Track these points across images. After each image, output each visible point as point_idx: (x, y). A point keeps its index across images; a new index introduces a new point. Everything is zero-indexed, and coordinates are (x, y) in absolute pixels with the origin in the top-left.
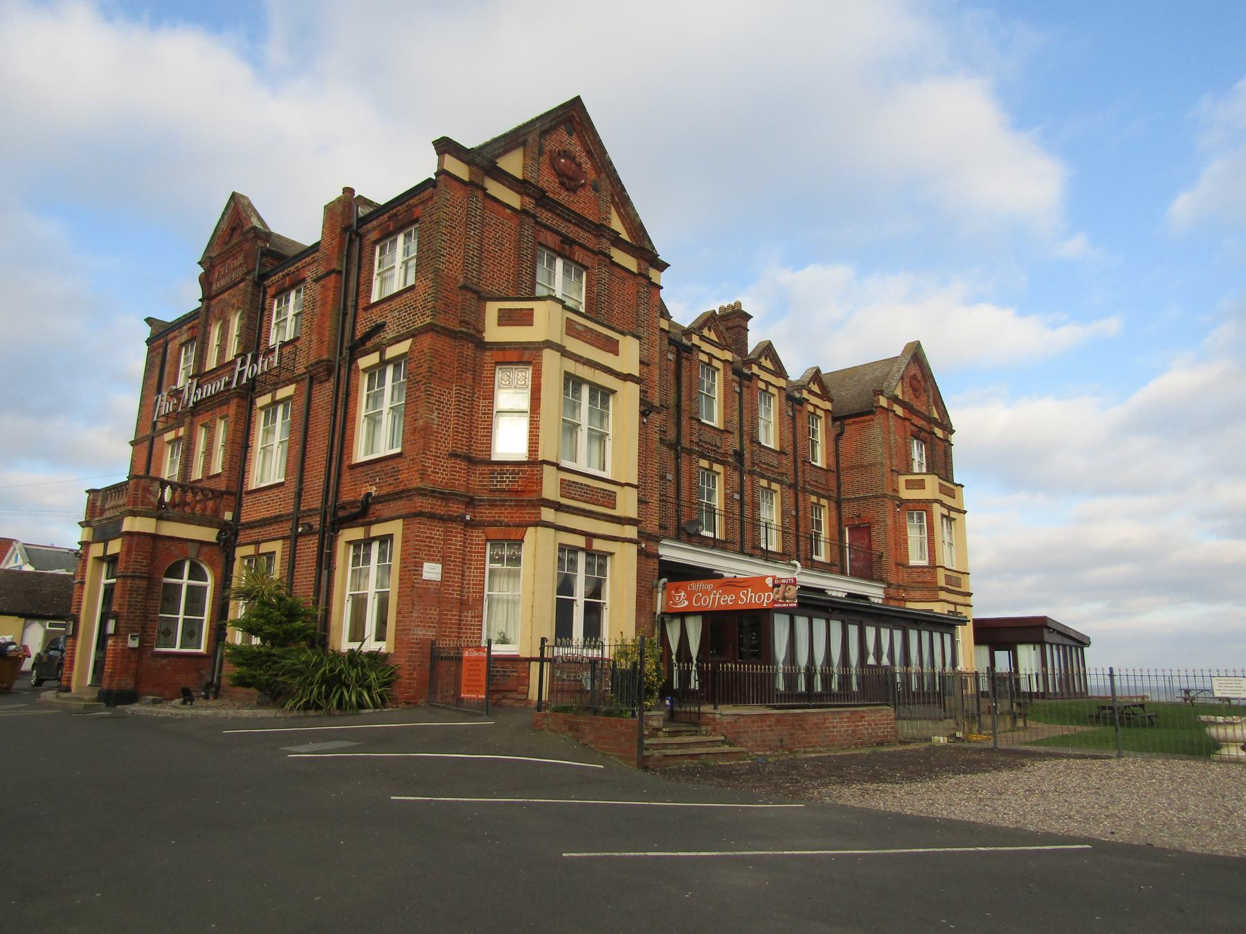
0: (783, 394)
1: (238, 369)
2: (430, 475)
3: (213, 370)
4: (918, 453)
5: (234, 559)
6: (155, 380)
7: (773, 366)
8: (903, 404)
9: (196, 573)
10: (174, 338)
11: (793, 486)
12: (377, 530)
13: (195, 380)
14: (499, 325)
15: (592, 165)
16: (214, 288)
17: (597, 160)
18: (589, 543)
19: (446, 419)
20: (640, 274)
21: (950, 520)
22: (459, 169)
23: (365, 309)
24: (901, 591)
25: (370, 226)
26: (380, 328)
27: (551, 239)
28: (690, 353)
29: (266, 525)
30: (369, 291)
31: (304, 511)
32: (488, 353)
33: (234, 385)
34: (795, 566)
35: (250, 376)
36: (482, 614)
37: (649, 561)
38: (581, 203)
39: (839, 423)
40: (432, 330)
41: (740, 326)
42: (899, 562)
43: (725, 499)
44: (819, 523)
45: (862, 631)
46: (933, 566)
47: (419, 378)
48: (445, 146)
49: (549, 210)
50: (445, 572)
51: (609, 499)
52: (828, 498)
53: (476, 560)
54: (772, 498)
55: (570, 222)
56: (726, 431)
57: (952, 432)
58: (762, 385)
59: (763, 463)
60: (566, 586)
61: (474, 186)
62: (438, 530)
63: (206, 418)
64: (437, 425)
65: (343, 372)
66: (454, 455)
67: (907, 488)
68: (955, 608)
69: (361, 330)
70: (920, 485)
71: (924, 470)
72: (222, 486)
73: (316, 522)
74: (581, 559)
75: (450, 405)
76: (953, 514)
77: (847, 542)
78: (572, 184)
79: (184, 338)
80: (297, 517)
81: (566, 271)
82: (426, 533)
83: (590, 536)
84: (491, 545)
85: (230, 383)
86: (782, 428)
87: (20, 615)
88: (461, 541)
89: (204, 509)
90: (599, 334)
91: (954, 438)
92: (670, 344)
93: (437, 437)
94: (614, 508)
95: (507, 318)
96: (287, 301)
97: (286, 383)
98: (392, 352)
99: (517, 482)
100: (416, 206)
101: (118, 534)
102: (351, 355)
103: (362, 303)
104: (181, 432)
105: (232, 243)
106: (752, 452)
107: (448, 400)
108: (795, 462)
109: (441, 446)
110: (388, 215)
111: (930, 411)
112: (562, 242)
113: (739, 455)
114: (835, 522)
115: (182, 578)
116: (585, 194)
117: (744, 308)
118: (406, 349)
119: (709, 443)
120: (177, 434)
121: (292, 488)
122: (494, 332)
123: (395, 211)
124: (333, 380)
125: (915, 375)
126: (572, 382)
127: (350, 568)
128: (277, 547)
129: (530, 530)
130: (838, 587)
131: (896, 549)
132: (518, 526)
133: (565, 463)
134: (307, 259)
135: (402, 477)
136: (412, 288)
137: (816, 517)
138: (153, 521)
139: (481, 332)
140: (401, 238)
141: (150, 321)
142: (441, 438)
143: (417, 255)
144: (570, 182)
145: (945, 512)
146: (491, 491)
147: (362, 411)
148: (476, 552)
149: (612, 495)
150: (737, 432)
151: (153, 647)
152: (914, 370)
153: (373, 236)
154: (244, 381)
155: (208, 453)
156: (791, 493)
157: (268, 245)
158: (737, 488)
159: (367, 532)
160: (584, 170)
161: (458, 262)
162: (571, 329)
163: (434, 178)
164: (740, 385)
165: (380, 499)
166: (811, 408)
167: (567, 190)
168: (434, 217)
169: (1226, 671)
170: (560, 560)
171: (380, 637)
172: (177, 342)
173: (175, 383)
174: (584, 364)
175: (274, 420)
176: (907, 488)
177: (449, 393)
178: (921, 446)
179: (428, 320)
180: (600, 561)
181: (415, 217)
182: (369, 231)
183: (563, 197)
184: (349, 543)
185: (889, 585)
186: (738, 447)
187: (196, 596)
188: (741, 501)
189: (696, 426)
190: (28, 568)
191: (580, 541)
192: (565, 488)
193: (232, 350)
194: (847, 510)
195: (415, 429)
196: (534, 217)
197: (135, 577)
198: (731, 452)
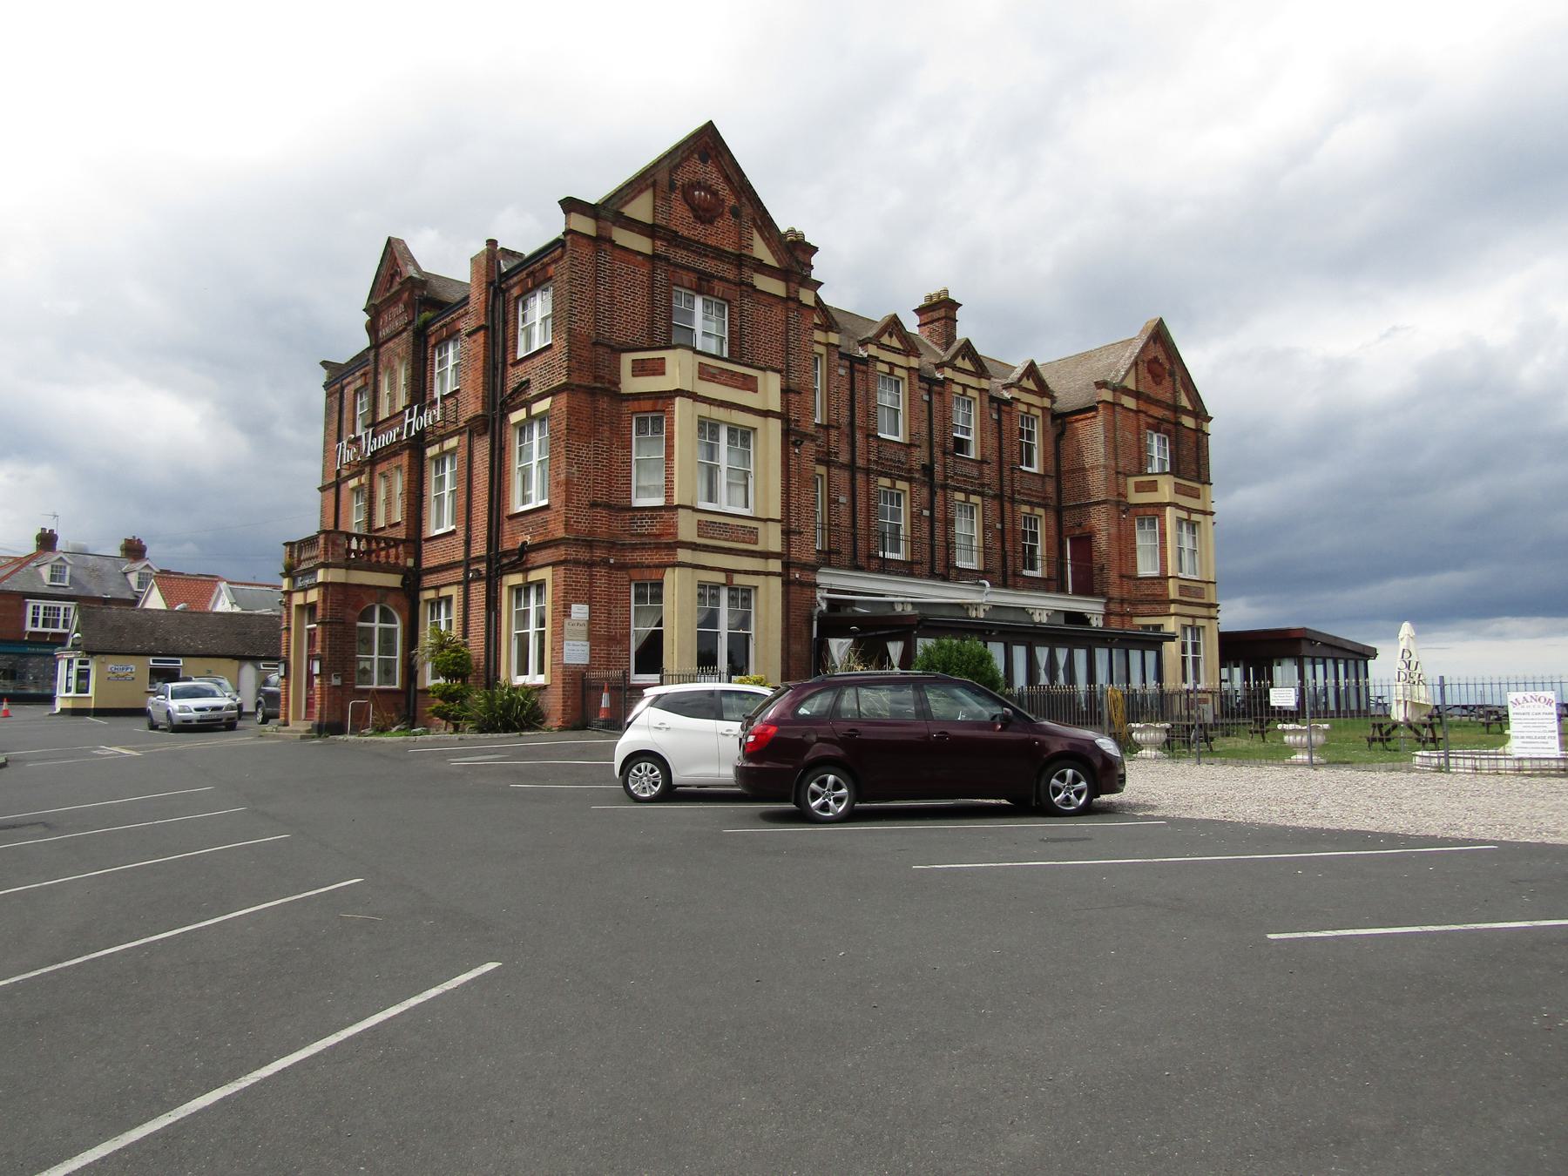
0: (986, 399)
1: (407, 421)
2: (573, 525)
3: (388, 419)
4: (1158, 450)
5: (419, 603)
6: (335, 426)
7: (973, 365)
8: (1136, 395)
9: (386, 617)
10: (349, 383)
11: (1000, 497)
12: (534, 576)
13: (371, 430)
14: (633, 376)
15: (731, 190)
17: (736, 184)
19: (585, 472)
20: (788, 298)
21: (1193, 526)
22: (586, 225)
23: (513, 365)
24: (1125, 606)
25: (512, 282)
26: (526, 384)
27: (687, 278)
28: (867, 365)
29: (443, 570)
30: (515, 346)
31: (473, 558)
32: (625, 404)
33: (405, 437)
34: (984, 585)
35: (418, 429)
36: (630, 648)
37: (805, 589)
38: (721, 235)
39: (1059, 421)
40: (567, 389)
42: (1124, 572)
43: (912, 517)
44: (1034, 536)
45: (1031, 654)
48: (570, 205)
49: (684, 249)
51: (753, 535)
53: (621, 600)
54: (972, 513)
55: (707, 256)
56: (910, 446)
59: (960, 475)
60: (711, 619)
61: (601, 241)
62: (584, 575)
64: (578, 478)
66: (594, 505)
67: (1137, 491)
68: (1194, 622)
69: (511, 385)
72: (401, 533)
73: (483, 567)
74: (724, 595)
75: (590, 458)
76: (1195, 517)
77: (1069, 557)
78: (708, 215)
79: (359, 383)
80: (467, 562)
81: (706, 305)
82: (572, 578)
83: (729, 572)
84: (636, 585)
85: (401, 434)
86: (984, 435)
87: (234, 657)
88: (605, 583)
89: (388, 556)
90: (734, 373)
91: (1211, 428)
92: (841, 358)
93: (577, 489)
94: (756, 543)
95: (641, 369)
96: (447, 351)
97: (451, 435)
98: (538, 408)
99: (656, 526)
100: (549, 264)
103: (510, 361)
104: (364, 479)
105: (393, 290)
107: (587, 454)
109: (583, 497)
110: (525, 272)
112: (699, 279)
113: (928, 470)
114: (1053, 533)
115: (373, 622)
116: (724, 223)
118: (547, 407)
119: (891, 460)
120: (360, 480)
121: (461, 534)
122: (632, 384)
123: (531, 268)
124: (489, 433)
125: (1156, 358)
126: (708, 428)
128: (454, 591)
129: (669, 570)
131: (1120, 560)
132: (658, 566)
134: (460, 311)
136: (549, 347)
137: (1031, 527)
138: (343, 571)
140: (539, 295)
141: (325, 364)
142: (582, 489)
143: (552, 314)
144: (705, 215)
145: (1184, 515)
146: (632, 535)
148: (621, 592)
149: (754, 532)
150: (925, 446)
151: (354, 684)
152: (1157, 352)
153: (515, 292)
154: (413, 433)
155: (389, 502)
157: (425, 293)
160: (722, 197)
161: (590, 319)
162: (705, 373)
163: (562, 237)
164: (930, 393)
166: (1023, 408)
167: (703, 223)
169: (1388, 680)
170: (700, 595)
171: (541, 671)
172: (352, 387)
173: (354, 432)
174: (719, 406)
175: (444, 471)
176: (1137, 491)
177: (588, 447)
178: (1164, 439)
179: (564, 380)
180: (744, 594)
181: (549, 275)
182: (512, 287)
183: (698, 232)
185: (1110, 600)
186: (927, 462)
187: (388, 636)
188: (932, 518)
189: (874, 444)
190: (237, 609)
191: (720, 578)
192: (702, 529)
193: (402, 401)
195: (558, 483)
196: (667, 259)
197: (333, 622)
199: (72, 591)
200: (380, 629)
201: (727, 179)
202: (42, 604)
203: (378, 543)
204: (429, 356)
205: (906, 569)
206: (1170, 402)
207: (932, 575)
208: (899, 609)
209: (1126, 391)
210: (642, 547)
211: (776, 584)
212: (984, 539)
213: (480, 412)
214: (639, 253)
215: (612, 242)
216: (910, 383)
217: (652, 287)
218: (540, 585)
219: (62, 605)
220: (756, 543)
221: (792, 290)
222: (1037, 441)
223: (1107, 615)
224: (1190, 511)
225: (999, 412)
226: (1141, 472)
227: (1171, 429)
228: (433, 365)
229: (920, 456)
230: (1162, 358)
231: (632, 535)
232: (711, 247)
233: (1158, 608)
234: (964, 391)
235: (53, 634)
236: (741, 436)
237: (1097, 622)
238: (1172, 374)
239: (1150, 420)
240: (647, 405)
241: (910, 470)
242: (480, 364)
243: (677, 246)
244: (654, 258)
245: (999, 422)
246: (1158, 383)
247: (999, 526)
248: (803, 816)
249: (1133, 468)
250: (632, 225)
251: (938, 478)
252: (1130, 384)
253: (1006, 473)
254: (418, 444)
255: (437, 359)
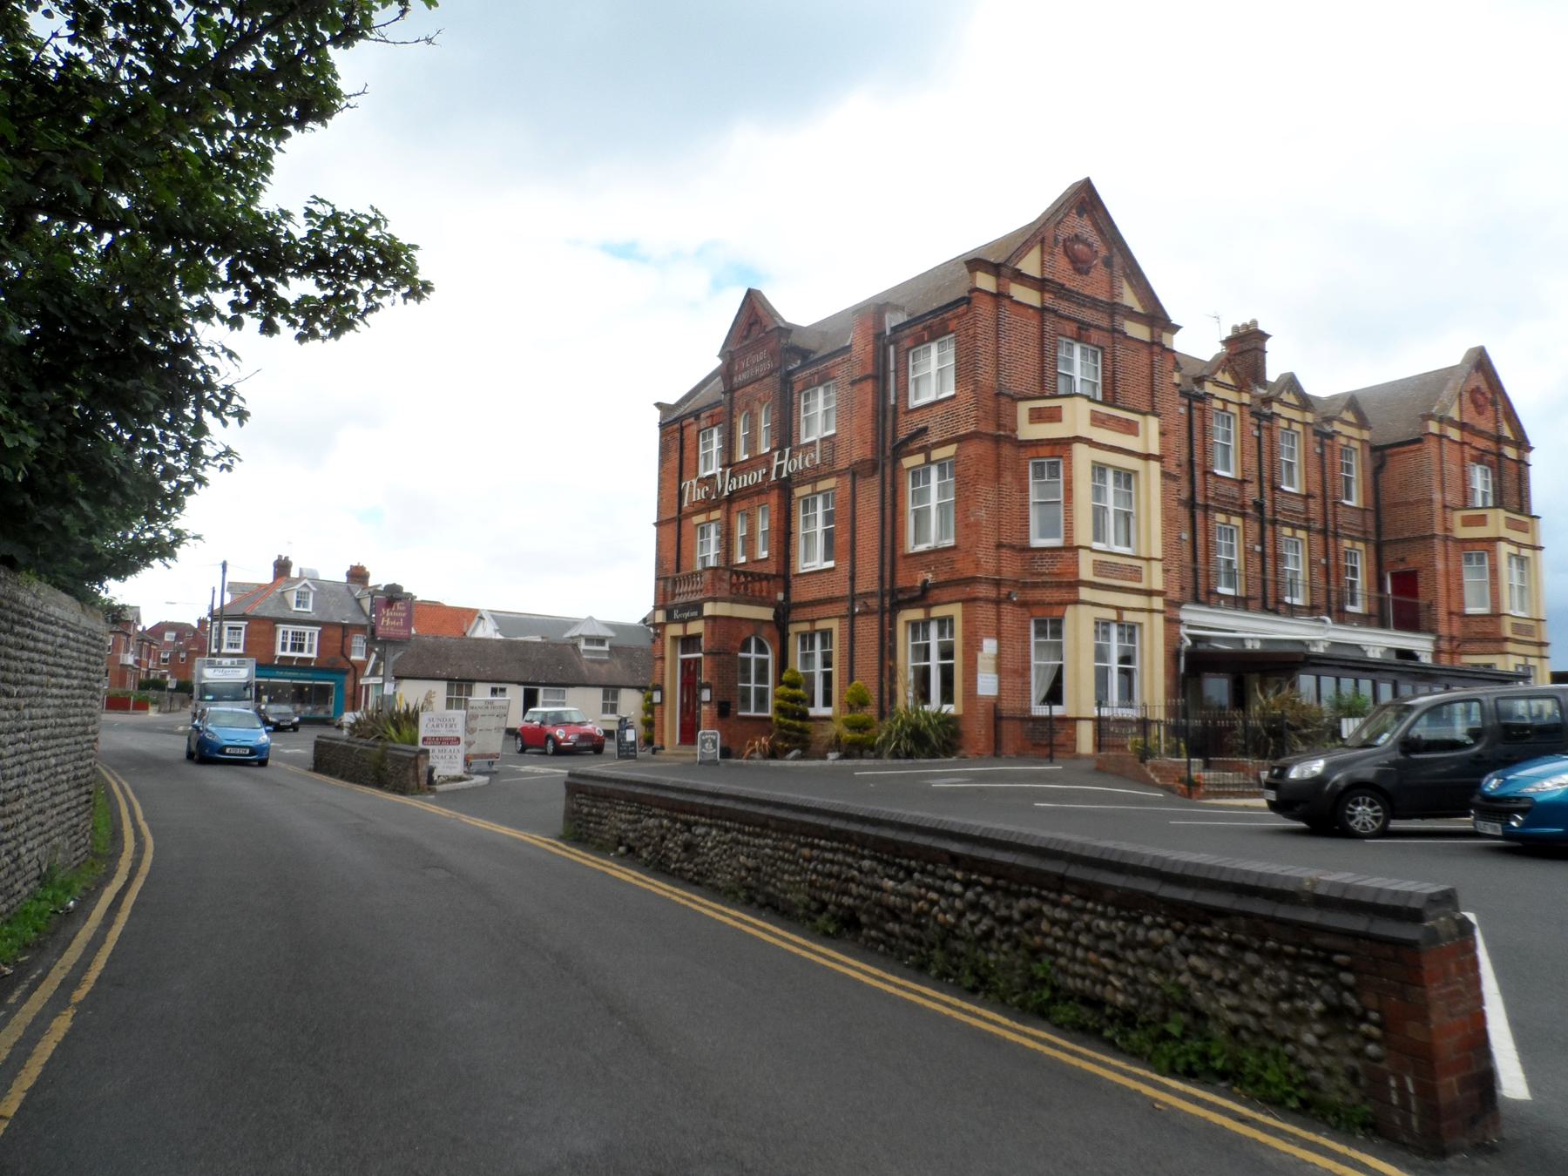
0: (1310, 431)
1: (776, 463)
4: (1480, 480)
8: (1462, 426)
9: (761, 648)
11: (1324, 532)
12: (937, 612)
13: (728, 471)
16: (735, 380)
18: (1120, 616)
26: (924, 430)
27: (1070, 328)
33: (773, 478)
34: (1324, 621)
38: (1094, 285)
41: (1256, 349)
42: (1454, 608)
43: (1246, 553)
44: (1354, 570)
46: (1496, 616)
47: (967, 480)
50: (1000, 646)
51: (1136, 573)
52: (1366, 541)
54: (1297, 547)
55: (1084, 306)
56: (1243, 482)
57: (1530, 449)
58: (1283, 423)
63: (744, 504)
65: (888, 470)
70: (1481, 521)
71: (1490, 503)
72: (772, 569)
74: (1114, 630)
76: (1525, 552)
80: (853, 598)
81: (1083, 354)
83: (1119, 609)
85: (768, 474)
91: (1532, 458)
94: (1140, 581)
95: (1038, 416)
98: (937, 454)
101: (700, 616)
102: (893, 455)
106: (1273, 501)
108: (1324, 504)
111: (1497, 428)
112: (1079, 328)
113: (1259, 506)
114: (1373, 568)
116: (1099, 273)
117: (1261, 327)
122: (1029, 431)
126: (1099, 469)
127: (910, 643)
130: (1378, 643)
133: (1097, 545)
135: (958, 566)
139: (1014, 431)
141: (659, 405)
144: (1080, 266)
145: (1514, 550)
146: (1033, 574)
147: (910, 507)
150: (1256, 481)
152: (1479, 381)
156: (1318, 539)
158: (1257, 540)
159: (928, 613)
164: (1259, 427)
165: (937, 586)
166: (1343, 441)
168: (971, 332)
170: (1096, 632)
171: (827, 702)
184: (907, 622)
185: (1439, 637)
188: (1263, 555)
191: (1112, 615)
194: (1389, 554)
196: (1055, 312)
198: (1250, 503)
199: (314, 616)
200: (757, 659)
201: (1100, 232)
202: (291, 628)
203: (738, 577)
204: (795, 401)
205: (1240, 603)
206: (1493, 432)
207: (1265, 608)
208: (1249, 645)
209: (1452, 422)
210: (1044, 585)
211: (1159, 620)
212: (1311, 574)
213: (869, 456)
214: (1031, 307)
215: (1010, 297)
216: (1242, 419)
217: (1042, 337)
218: (945, 623)
219: (307, 629)
220: (1140, 581)
221: (1156, 335)
222: (1356, 475)
223: (1437, 653)
224: (1520, 545)
225: (1322, 445)
226: (1465, 507)
227: (1496, 462)
228: (799, 409)
229: (1252, 491)
230: (1484, 387)
231: (1033, 574)
232: (1087, 297)
233: (1491, 646)
234: (1290, 425)
235: (300, 659)
236: (1126, 478)
237: (1426, 659)
238: (1494, 403)
239: (1474, 452)
240: (1045, 451)
241: (1243, 506)
242: (869, 409)
243: (1061, 298)
244: (1043, 311)
245: (1322, 456)
246: (1480, 413)
247: (1323, 561)
248: (1348, 834)
249: (1458, 501)
250: (1020, 277)
251: (1268, 514)
252: (1454, 413)
253: (1330, 507)
254: (785, 487)
255: (803, 404)
